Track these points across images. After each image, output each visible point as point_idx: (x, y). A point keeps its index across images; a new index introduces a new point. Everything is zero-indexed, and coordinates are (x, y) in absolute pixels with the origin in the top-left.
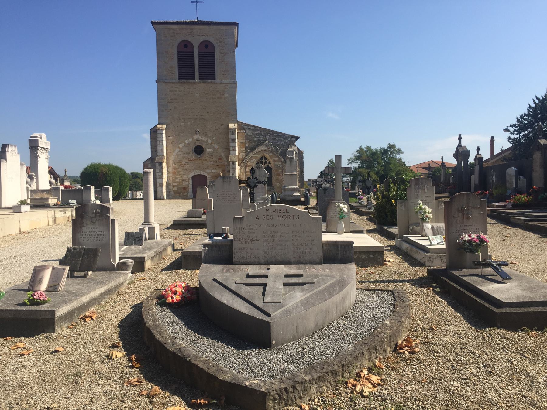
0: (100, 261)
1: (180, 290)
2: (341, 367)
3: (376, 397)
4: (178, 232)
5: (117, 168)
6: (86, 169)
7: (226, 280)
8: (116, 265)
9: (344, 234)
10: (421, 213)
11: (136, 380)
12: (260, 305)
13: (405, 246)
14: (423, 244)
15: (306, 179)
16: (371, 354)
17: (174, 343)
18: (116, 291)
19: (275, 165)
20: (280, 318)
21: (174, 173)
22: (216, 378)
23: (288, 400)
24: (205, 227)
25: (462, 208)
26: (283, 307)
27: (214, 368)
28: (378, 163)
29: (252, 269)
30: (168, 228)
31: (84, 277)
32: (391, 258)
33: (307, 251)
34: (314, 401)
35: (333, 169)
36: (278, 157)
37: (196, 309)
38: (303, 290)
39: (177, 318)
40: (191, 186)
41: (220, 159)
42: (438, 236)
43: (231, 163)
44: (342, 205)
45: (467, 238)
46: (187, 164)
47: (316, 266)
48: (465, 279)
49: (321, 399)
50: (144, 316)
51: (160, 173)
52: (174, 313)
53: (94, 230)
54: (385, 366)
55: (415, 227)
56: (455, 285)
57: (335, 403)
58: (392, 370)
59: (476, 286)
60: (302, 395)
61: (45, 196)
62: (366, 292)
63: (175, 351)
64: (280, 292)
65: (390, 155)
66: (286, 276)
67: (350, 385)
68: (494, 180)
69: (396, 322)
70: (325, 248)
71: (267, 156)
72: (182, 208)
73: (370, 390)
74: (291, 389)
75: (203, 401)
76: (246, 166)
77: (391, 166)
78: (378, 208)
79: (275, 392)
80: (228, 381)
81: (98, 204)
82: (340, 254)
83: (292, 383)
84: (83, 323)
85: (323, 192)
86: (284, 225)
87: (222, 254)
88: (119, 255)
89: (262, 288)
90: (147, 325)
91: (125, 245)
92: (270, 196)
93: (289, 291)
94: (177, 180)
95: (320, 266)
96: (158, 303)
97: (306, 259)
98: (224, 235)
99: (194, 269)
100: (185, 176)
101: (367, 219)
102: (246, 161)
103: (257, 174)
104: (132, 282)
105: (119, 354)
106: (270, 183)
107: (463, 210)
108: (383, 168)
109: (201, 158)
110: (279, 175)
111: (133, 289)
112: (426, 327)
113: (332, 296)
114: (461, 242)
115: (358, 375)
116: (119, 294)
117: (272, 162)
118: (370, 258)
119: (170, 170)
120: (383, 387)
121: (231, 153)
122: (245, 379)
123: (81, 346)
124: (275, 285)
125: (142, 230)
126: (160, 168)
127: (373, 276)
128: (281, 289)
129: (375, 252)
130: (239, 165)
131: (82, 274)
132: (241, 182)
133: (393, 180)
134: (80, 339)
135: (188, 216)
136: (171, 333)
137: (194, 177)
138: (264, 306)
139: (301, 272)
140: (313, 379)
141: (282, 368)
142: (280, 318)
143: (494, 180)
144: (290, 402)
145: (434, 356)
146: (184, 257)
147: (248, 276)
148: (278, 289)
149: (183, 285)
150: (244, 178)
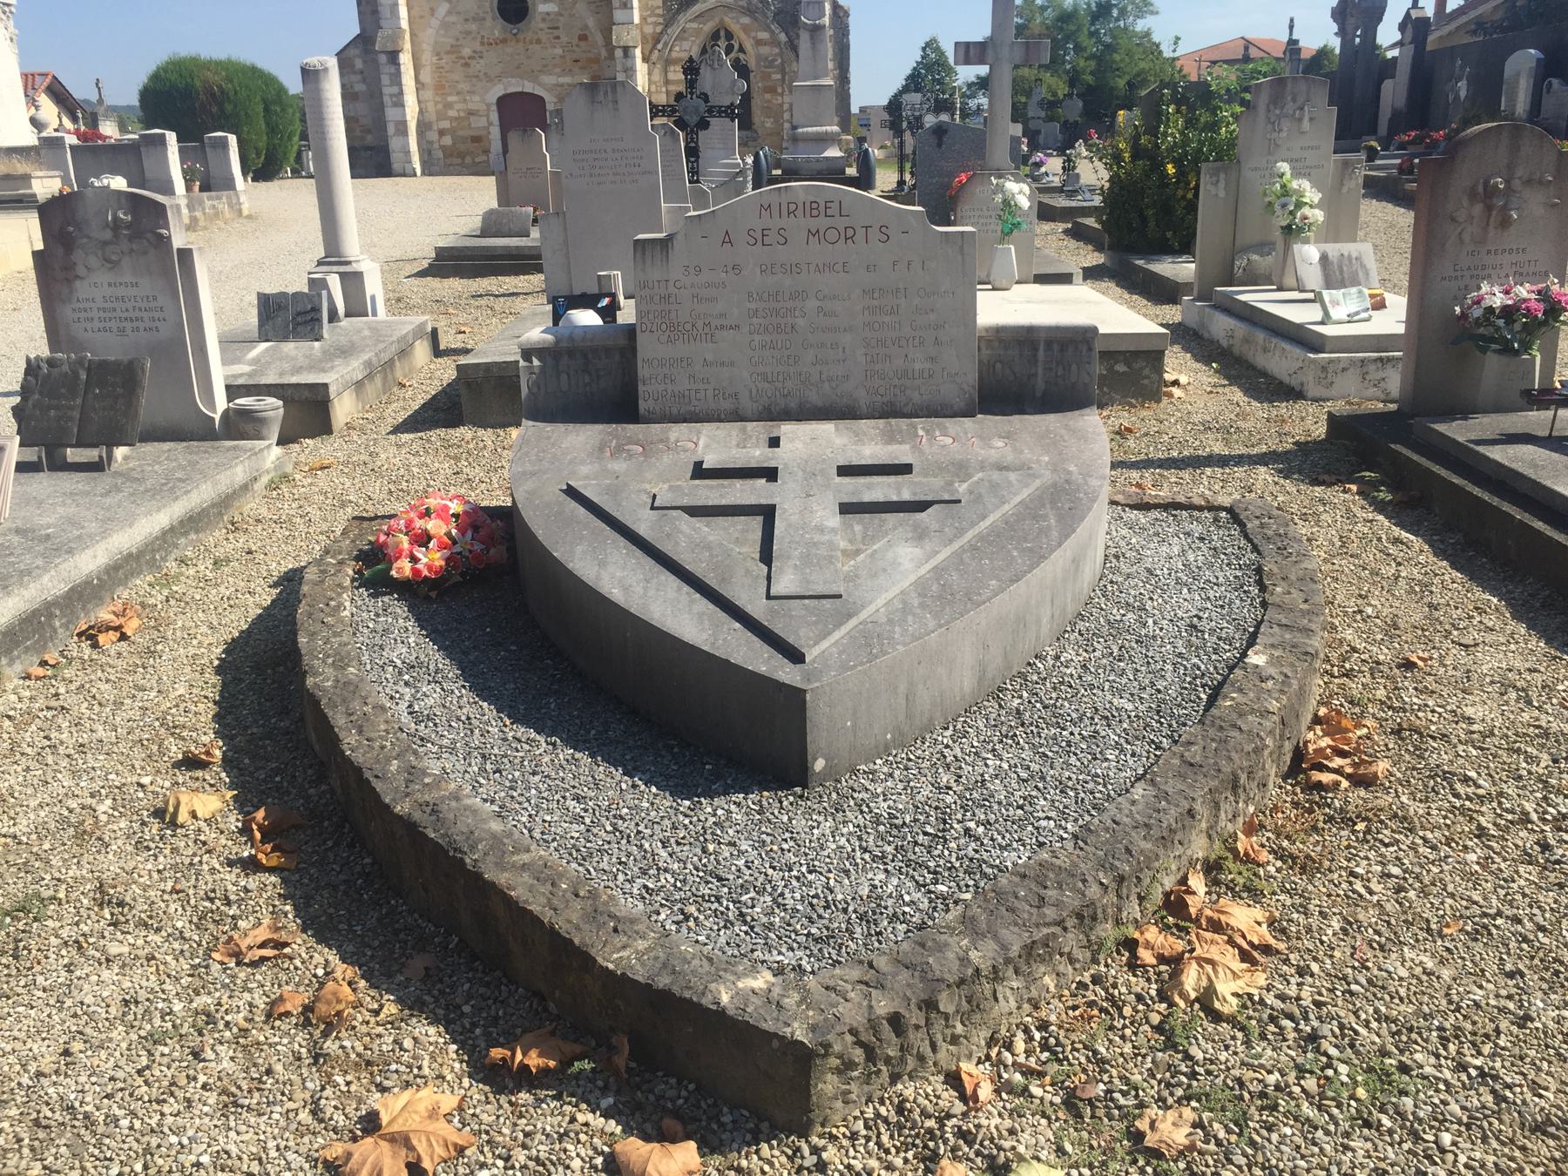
0: (150, 404)
1: (444, 530)
2: (1114, 885)
3: (1272, 1019)
4: (455, 285)
5: (254, 72)
6: (156, 77)
7: (614, 491)
8: (217, 417)
9: (1016, 287)
10: (1284, 206)
11: (263, 934)
12: (756, 607)
13: (1221, 326)
14: (1297, 321)
15: (855, 109)
16: (1217, 806)
17: (413, 773)
18: (221, 514)
19: (759, 57)
20: (844, 667)
21: (439, 88)
22: (585, 960)
23: (902, 1060)
24: (538, 269)
25: (1486, 183)
26: (850, 616)
27: (577, 905)
28: (1078, 49)
29: (717, 444)
30: (422, 274)
31: (96, 467)
32: (1179, 367)
33: (918, 366)
34: (1009, 1046)
35: (928, 74)
36: (767, 28)
37: (506, 610)
38: (920, 535)
39: (431, 648)
40: (495, 132)
41: (583, 38)
42: (1354, 290)
43: (619, 53)
44: (1012, 186)
45: (1498, 301)
46: (477, 55)
47: (953, 425)
48: (1496, 454)
49: (1037, 1036)
50: (302, 640)
51: (395, 90)
52: (422, 622)
53: (121, 291)
54: (1272, 851)
55: (1255, 257)
56: (1456, 480)
57: (1104, 1061)
58: (1303, 869)
59: (1548, 483)
60: (959, 1029)
61: (20, 167)
62: (1134, 515)
63: (417, 816)
64: (832, 546)
65: (1117, 20)
66: (844, 471)
67: (1146, 956)
68: (1463, 94)
69: (1292, 659)
70: (985, 352)
71: (735, 28)
72: (460, 206)
73: (1239, 986)
74: (915, 1017)
75: (534, 1060)
76: (668, 62)
77: (1117, 57)
78: (1120, 196)
79: (849, 1038)
80: (640, 975)
81: (119, 192)
82: (1037, 377)
83: (919, 991)
84: (87, 651)
85: (933, 140)
86: (831, 267)
87: (597, 384)
88: (226, 377)
89: (756, 523)
90: (310, 681)
91: (264, 338)
92: (750, 160)
93: (868, 539)
94: (453, 113)
95: (967, 422)
96: (361, 581)
97: (916, 397)
98: (605, 302)
99: (504, 426)
100: (476, 98)
101: (1066, 232)
102: (666, 44)
103: (706, 81)
104: (285, 478)
105: (207, 802)
106: (743, 114)
107: (1490, 192)
108: (1093, 63)
109: (521, 36)
110: (772, 90)
111: (289, 508)
112: (1384, 655)
113: (1037, 557)
114: (1477, 312)
115: (1175, 905)
116: (235, 527)
117: (748, 45)
118: (1128, 372)
119: (426, 77)
120: (1286, 961)
121: (619, 15)
122: (722, 968)
123: (64, 763)
124: (808, 511)
125: (317, 285)
126: (393, 70)
127: (1131, 443)
128: (833, 530)
129: (1136, 354)
130: (645, 59)
131: (90, 454)
132: (656, 111)
133: (1175, 92)
134: (66, 737)
135: (485, 232)
136: (405, 719)
137: (503, 102)
138: (772, 611)
139: (900, 453)
140: (1008, 961)
141: (865, 891)
142: (844, 667)
143: (1463, 94)
144: (911, 1063)
145: (1457, 796)
146: (469, 385)
147: (700, 472)
148: (821, 529)
149: (455, 507)
150: (662, 99)
